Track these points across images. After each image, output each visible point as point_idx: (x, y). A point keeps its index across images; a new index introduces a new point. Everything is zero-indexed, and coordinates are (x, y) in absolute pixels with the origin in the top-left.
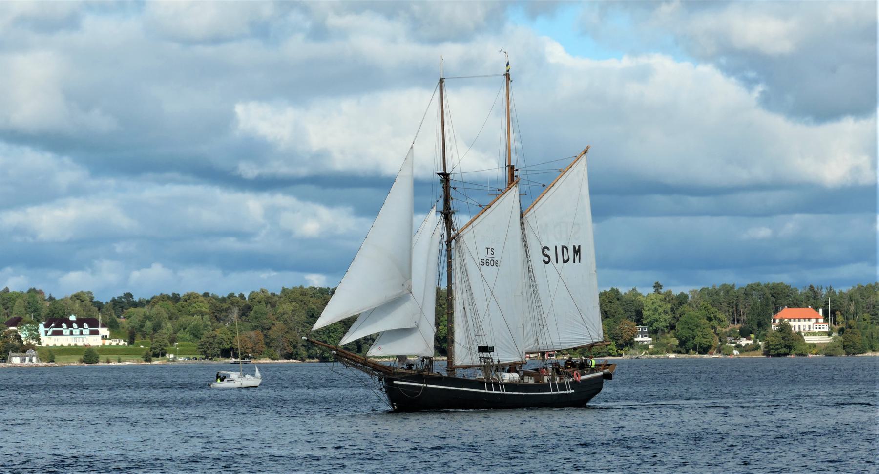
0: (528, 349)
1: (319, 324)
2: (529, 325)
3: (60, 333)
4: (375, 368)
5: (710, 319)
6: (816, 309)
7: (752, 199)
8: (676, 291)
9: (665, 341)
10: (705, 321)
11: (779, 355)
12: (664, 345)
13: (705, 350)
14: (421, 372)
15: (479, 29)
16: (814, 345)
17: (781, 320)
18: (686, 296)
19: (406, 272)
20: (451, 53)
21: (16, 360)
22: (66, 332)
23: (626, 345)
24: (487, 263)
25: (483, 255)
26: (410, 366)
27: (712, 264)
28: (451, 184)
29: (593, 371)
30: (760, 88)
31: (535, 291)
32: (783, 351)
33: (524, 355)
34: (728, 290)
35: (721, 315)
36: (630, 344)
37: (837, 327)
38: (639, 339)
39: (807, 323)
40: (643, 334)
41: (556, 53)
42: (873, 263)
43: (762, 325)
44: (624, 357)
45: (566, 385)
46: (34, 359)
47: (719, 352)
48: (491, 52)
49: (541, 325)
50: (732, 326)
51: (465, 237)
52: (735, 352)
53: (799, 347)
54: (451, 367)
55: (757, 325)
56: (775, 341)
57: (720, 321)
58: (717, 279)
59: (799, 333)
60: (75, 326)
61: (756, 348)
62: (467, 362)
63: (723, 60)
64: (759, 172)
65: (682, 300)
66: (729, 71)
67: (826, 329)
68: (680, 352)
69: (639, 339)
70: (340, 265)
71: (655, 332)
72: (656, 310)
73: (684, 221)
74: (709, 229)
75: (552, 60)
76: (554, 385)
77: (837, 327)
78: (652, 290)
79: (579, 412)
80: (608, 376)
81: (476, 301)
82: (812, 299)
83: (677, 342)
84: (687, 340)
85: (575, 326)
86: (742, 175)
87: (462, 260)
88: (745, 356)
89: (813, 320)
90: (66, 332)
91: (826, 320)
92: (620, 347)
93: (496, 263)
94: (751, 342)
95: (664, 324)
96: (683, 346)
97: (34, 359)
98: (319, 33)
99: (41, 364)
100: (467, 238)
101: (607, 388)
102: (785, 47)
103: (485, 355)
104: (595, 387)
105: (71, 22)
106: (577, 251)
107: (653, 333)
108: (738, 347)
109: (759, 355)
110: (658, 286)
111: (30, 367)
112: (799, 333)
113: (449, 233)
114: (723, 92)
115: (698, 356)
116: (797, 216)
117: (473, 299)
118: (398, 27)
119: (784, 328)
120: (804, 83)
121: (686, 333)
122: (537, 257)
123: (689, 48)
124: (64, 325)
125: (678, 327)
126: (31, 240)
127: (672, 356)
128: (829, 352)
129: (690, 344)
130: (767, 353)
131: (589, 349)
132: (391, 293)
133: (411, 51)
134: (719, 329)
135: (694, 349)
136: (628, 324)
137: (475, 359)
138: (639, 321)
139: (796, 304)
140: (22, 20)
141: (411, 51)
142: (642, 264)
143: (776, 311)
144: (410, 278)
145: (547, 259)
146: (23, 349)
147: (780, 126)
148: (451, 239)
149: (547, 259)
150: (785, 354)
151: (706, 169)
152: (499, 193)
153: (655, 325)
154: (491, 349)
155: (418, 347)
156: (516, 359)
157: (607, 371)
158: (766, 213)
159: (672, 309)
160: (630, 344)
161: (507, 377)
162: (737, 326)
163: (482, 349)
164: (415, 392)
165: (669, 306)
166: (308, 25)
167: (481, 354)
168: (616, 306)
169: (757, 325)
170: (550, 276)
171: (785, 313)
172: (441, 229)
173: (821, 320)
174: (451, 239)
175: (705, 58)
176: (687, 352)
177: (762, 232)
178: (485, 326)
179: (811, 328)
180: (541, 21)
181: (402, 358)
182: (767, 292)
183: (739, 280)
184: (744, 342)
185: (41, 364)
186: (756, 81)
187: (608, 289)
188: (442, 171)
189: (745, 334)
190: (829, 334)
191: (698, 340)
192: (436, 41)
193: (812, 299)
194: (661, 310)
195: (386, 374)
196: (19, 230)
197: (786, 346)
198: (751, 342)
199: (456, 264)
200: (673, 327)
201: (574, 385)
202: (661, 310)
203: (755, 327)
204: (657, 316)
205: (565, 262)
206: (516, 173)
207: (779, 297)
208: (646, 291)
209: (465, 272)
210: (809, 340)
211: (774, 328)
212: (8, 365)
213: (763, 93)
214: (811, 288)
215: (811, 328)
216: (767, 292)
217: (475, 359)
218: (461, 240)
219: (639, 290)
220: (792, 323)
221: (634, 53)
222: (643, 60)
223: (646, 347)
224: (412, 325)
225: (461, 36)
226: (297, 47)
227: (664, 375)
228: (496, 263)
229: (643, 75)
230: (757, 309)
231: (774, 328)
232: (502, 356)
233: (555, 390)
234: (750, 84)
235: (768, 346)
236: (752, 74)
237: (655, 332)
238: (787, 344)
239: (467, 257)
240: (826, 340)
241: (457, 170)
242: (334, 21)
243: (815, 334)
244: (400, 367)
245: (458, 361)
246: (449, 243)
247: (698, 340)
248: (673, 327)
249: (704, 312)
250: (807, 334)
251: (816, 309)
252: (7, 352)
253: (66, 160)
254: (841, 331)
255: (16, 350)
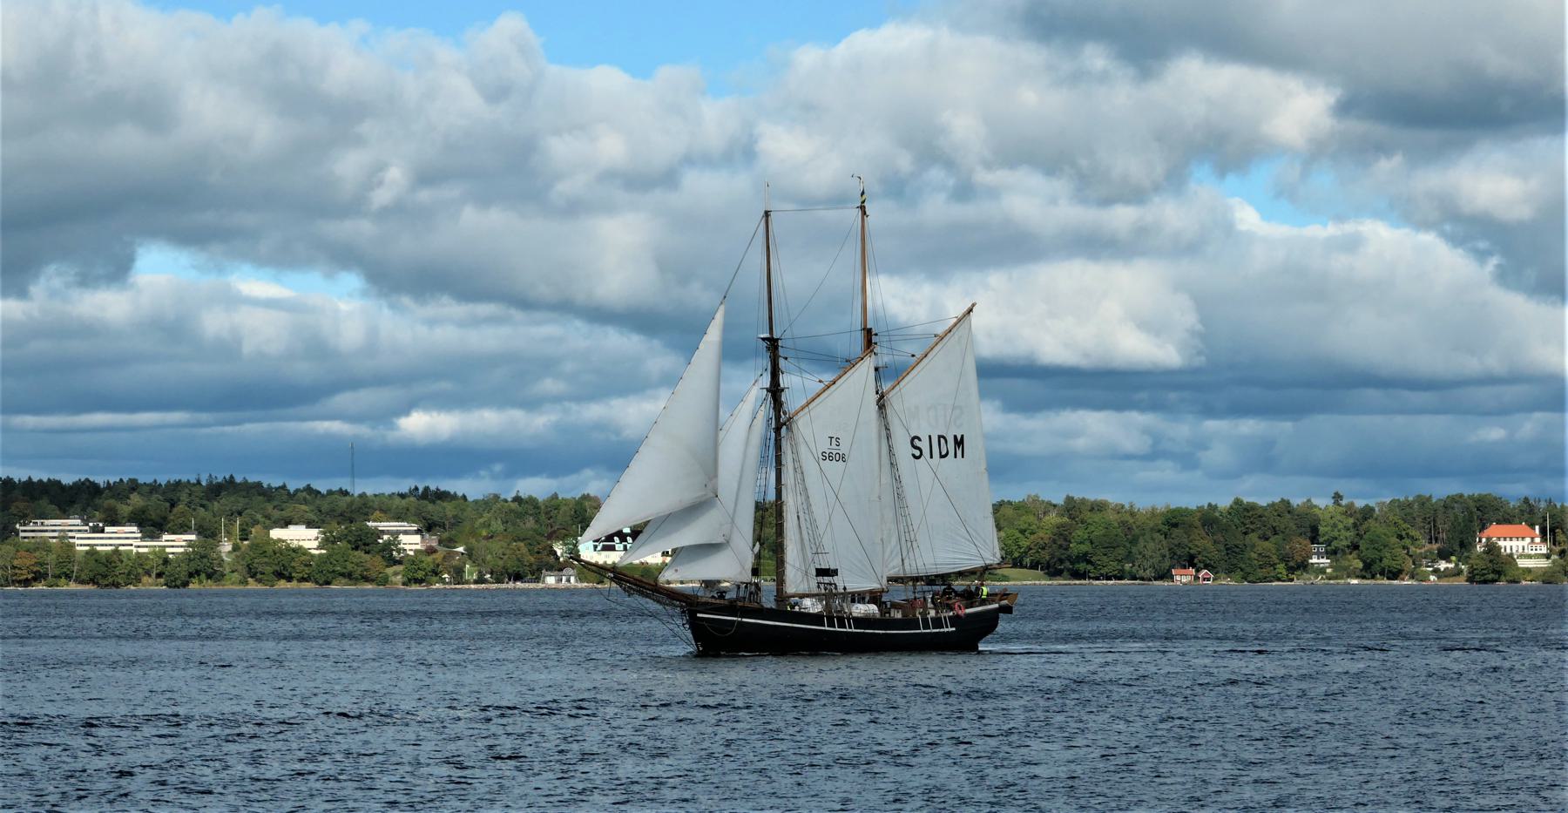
0: (893, 573)
1: (276, 533)
2: (894, 540)
3: (612, 548)
4: (672, 596)
5: (1401, 537)
6: (1532, 526)
7: (1484, 394)
8: (1360, 503)
9: (1346, 563)
10: (1394, 540)
11: (1485, 582)
12: (1345, 569)
13: (1394, 575)
14: (744, 602)
15: (1157, 188)
16: (1529, 570)
17: (1488, 539)
18: (1372, 510)
19: (711, 469)
20: (1122, 217)
21: (551, 580)
22: (619, 547)
23: (1298, 568)
24: (830, 457)
25: (825, 446)
26: (722, 594)
27: (1433, 471)
28: (781, 352)
29: (983, 602)
30: (1494, 261)
31: (899, 496)
32: (1490, 576)
33: (884, 581)
34: (1423, 502)
35: (1413, 533)
36: (1303, 566)
37: (1558, 549)
38: (1314, 560)
39: (1521, 543)
40: (1319, 555)
41: (1247, 217)
42: (1559, 473)
43: (1465, 545)
44: (1296, 582)
45: (942, 621)
46: (572, 579)
47: (1412, 577)
48: (1171, 214)
49: (907, 541)
50: (1428, 546)
51: (800, 423)
52: (1432, 578)
53: (1511, 574)
54: (781, 597)
55: (1459, 545)
56: (1481, 565)
57: (1414, 539)
58: (1409, 490)
59: (1511, 555)
60: (629, 539)
61: (1459, 573)
62: (803, 589)
63: (1448, 228)
64: (1493, 362)
65: (1367, 513)
66: (1455, 241)
67: (1544, 551)
68: (1364, 577)
69: (1314, 560)
70: (617, 458)
71: (1335, 552)
72: (1335, 526)
73: (1400, 420)
74: (1429, 430)
75: (1242, 227)
76: (925, 621)
77: (1558, 549)
78: (1330, 502)
79: (960, 658)
80: (1007, 610)
81: (814, 508)
82: (1526, 514)
83: (1361, 565)
84: (1373, 561)
85: (956, 540)
86: (1472, 365)
87: (795, 452)
88: (1444, 583)
89: (1528, 540)
90: (619, 547)
91: (1544, 540)
92: (1291, 570)
93: (843, 458)
94: (1451, 566)
95: (1345, 543)
96: (1368, 570)
97: (572, 579)
98: (964, 191)
99: (580, 585)
100: (802, 425)
101: (1003, 626)
102: (1524, 212)
103: (827, 579)
104: (986, 624)
105: (668, 178)
106: (959, 443)
107: (1332, 553)
108: (1436, 571)
109: (1461, 581)
110: (1337, 497)
111: (567, 589)
112: (1511, 555)
113: (778, 417)
114: (1448, 265)
115: (1387, 582)
116: (1538, 415)
117: (809, 505)
118: (1060, 186)
119: (1492, 549)
120: (1520, 252)
121: (1371, 554)
122: (903, 450)
123: (1406, 212)
124: (616, 539)
125: (1363, 545)
126: (613, 438)
127: (1355, 581)
128: (1548, 578)
129: (1376, 568)
130: (1471, 580)
131: (985, 572)
132: (688, 496)
133: (1071, 213)
134: (1412, 549)
135: (1382, 574)
136: (1300, 544)
137: (812, 584)
138: (1314, 540)
139: (1507, 520)
140: (610, 176)
141: (1071, 213)
142: (1350, 471)
143: (1483, 528)
144: (716, 476)
145: (917, 453)
146: (558, 567)
147: (1518, 307)
148: (780, 422)
149: (917, 453)
150: (1494, 581)
151: (1429, 359)
152: (850, 363)
153: (1335, 544)
154: (834, 573)
155: (730, 568)
156: (875, 586)
157: (1004, 602)
158: (1502, 411)
159: (1355, 525)
160: (1303, 566)
161: (860, 609)
162: (1435, 546)
163: (821, 572)
164: (730, 628)
165: (1351, 521)
166: (951, 182)
167: (820, 579)
168: (1009, 512)
169: (1459, 545)
170: (920, 476)
171: (1494, 530)
172: (766, 411)
173: (1538, 540)
174: (780, 422)
175: (1423, 225)
176: (1373, 577)
177: (1494, 433)
178: (826, 541)
179: (1525, 549)
180: (1232, 180)
181: (709, 584)
182: (1472, 504)
183: (1440, 490)
184: (1443, 565)
185: (580, 585)
186: (1489, 253)
187: (1277, 500)
188: (767, 335)
189: (1443, 555)
190: (1548, 557)
191: (1386, 562)
192: (1107, 202)
193: (1526, 514)
194: (1341, 526)
195: (686, 604)
196: (600, 426)
197: (1494, 571)
198: (1451, 566)
199: (788, 459)
200: (1355, 547)
201: (955, 620)
202: (1341, 526)
203: (1457, 548)
204: (1336, 534)
205: (942, 457)
206: (874, 339)
207: (1486, 511)
208: (1323, 502)
209: (799, 470)
210: (1523, 563)
211: (1479, 549)
212: (541, 585)
213: (1498, 266)
214: (1526, 500)
215: (1525, 549)
216: (1472, 504)
217: (812, 584)
218: (794, 427)
219: (1315, 501)
220: (1501, 543)
221: (1340, 218)
222: (1349, 227)
223: (1322, 571)
224: (720, 540)
225: (1135, 195)
226: (936, 209)
227: (1349, 605)
228: (843, 458)
229: (1352, 244)
230: (1460, 525)
231: (1479, 549)
232: (849, 581)
233: (926, 626)
234: (1482, 256)
235: (1472, 571)
236: (1482, 245)
237: (1335, 552)
238: (1497, 568)
239: (803, 449)
240: (1543, 563)
241: (788, 335)
242: (983, 177)
243: (1530, 557)
244: (706, 596)
245: (790, 589)
246: (778, 430)
247: (1386, 562)
248: (1355, 547)
249: (1394, 529)
250: (1520, 556)
251: (1532, 526)
252: (539, 570)
253: (656, 343)
254: (1562, 553)
255: (550, 568)
